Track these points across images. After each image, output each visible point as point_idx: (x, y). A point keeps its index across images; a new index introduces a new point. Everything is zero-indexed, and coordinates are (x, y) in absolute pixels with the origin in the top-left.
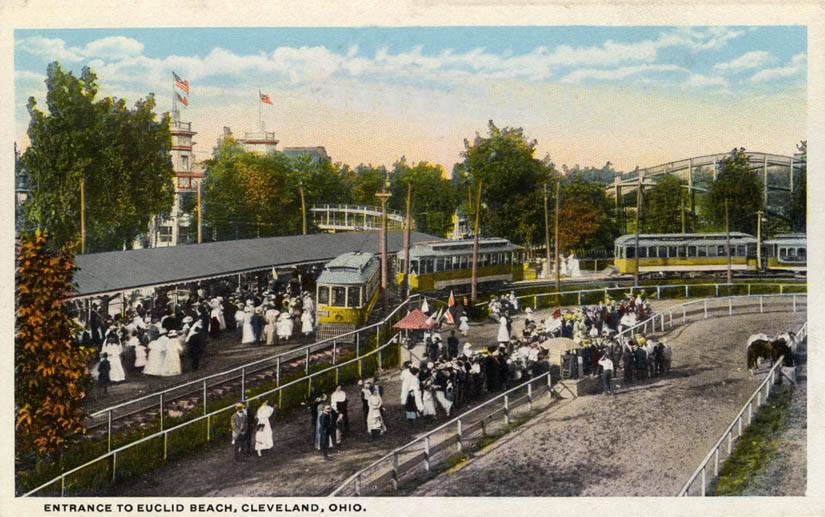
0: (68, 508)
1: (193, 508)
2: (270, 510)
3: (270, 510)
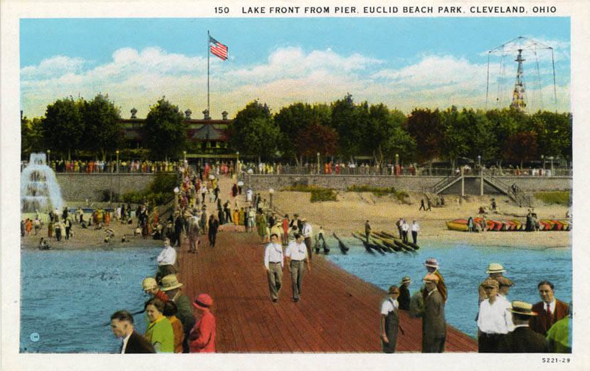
1: (522, 10)
2: (491, 11)
3: (491, 11)
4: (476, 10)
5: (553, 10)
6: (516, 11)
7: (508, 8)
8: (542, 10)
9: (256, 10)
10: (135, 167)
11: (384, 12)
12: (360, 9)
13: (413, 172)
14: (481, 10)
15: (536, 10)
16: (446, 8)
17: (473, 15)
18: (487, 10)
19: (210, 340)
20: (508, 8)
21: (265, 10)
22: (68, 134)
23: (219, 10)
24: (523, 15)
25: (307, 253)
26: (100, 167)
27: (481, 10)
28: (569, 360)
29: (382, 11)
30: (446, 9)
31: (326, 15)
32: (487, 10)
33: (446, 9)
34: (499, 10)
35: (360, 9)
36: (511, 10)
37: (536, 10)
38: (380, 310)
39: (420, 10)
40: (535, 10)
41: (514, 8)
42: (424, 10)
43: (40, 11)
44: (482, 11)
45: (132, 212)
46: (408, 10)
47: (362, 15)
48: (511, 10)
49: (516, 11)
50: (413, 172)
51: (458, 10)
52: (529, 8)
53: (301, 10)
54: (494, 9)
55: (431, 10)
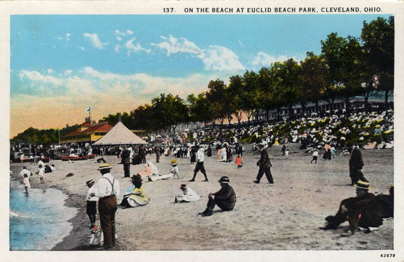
0: (200, 10)
1: (357, 10)
2: (335, 11)
3: (335, 11)
5: (378, 10)
6: (353, 11)
7: (348, 8)
8: (371, 10)
10: (344, 77)
11: (261, 12)
12: (235, 10)
14: (329, 10)
15: (366, 10)
16: (305, 8)
17: (185, 13)
18: (333, 10)
21: (208, 10)
24: (358, 13)
25: (27, 163)
26: (122, 147)
27: (263, 10)
29: (260, 11)
30: (305, 10)
31: (191, 13)
32: (333, 10)
33: (305, 10)
36: (350, 10)
39: (224, 10)
40: (366, 10)
41: (351, 9)
44: (264, 11)
45: (216, 123)
46: (216, 10)
47: (320, 13)
48: (350, 10)
49: (353, 11)
51: (313, 10)
52: (362, 9)
53: (245, 10)
54: (338, 9)
55: (293, 10)
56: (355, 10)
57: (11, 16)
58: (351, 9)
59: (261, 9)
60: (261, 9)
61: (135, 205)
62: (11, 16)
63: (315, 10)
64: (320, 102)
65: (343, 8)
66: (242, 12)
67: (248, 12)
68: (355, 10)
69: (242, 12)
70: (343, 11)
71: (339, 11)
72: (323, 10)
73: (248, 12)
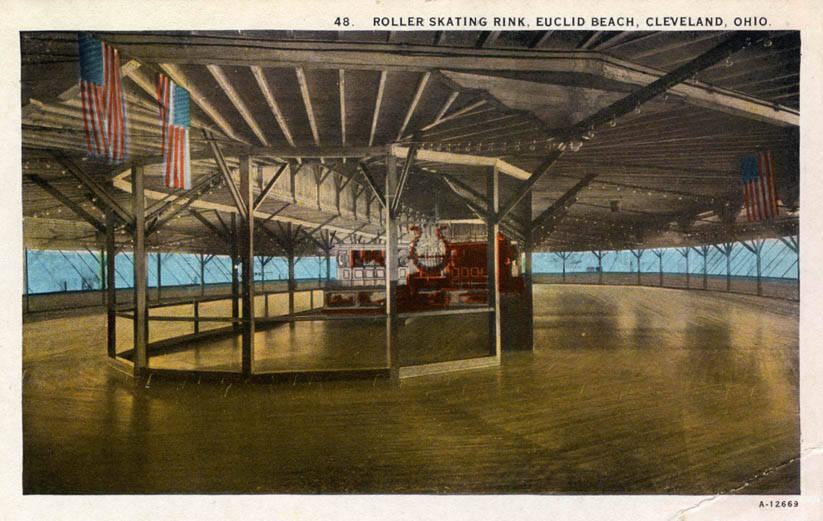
2: (675, 24)
3: (675, 24)
4: (562, 22)
5: (763, 22)
7: (700, 19)
9: (440, 21)
13: (497, 21)
19: (122, 304)
20: (700, 19)
22: (783, 479)
23: (376, 21)
28: (797, 504)
29: (655, 23)
33: (612, 21)
34: (687, 22)
35: (445, 21)
36: (704, 22)
37: (738, 22)
38: (510, 272)
41: (707, 19)
42: (621, 22)
43: (801, 34)
48: (704, 22)
49: (510, 19)
50: (497, 21)
54: (679, 20)
56: (714, 23)
57: (26, 492)
58: (707, 19)
59: (565, 20)
60: (565, 20)
61: (172, 83)
62: (26, 492)
63: (524, 21)
64: (229, 327)
65: (690, 19)
66: (458, 24)
67: (538, 25)
68: (714, 23)
69: (458, 24)
70: (690, 25)
71: (682, 24)
72: (650, 22)
73: (538, 25)
